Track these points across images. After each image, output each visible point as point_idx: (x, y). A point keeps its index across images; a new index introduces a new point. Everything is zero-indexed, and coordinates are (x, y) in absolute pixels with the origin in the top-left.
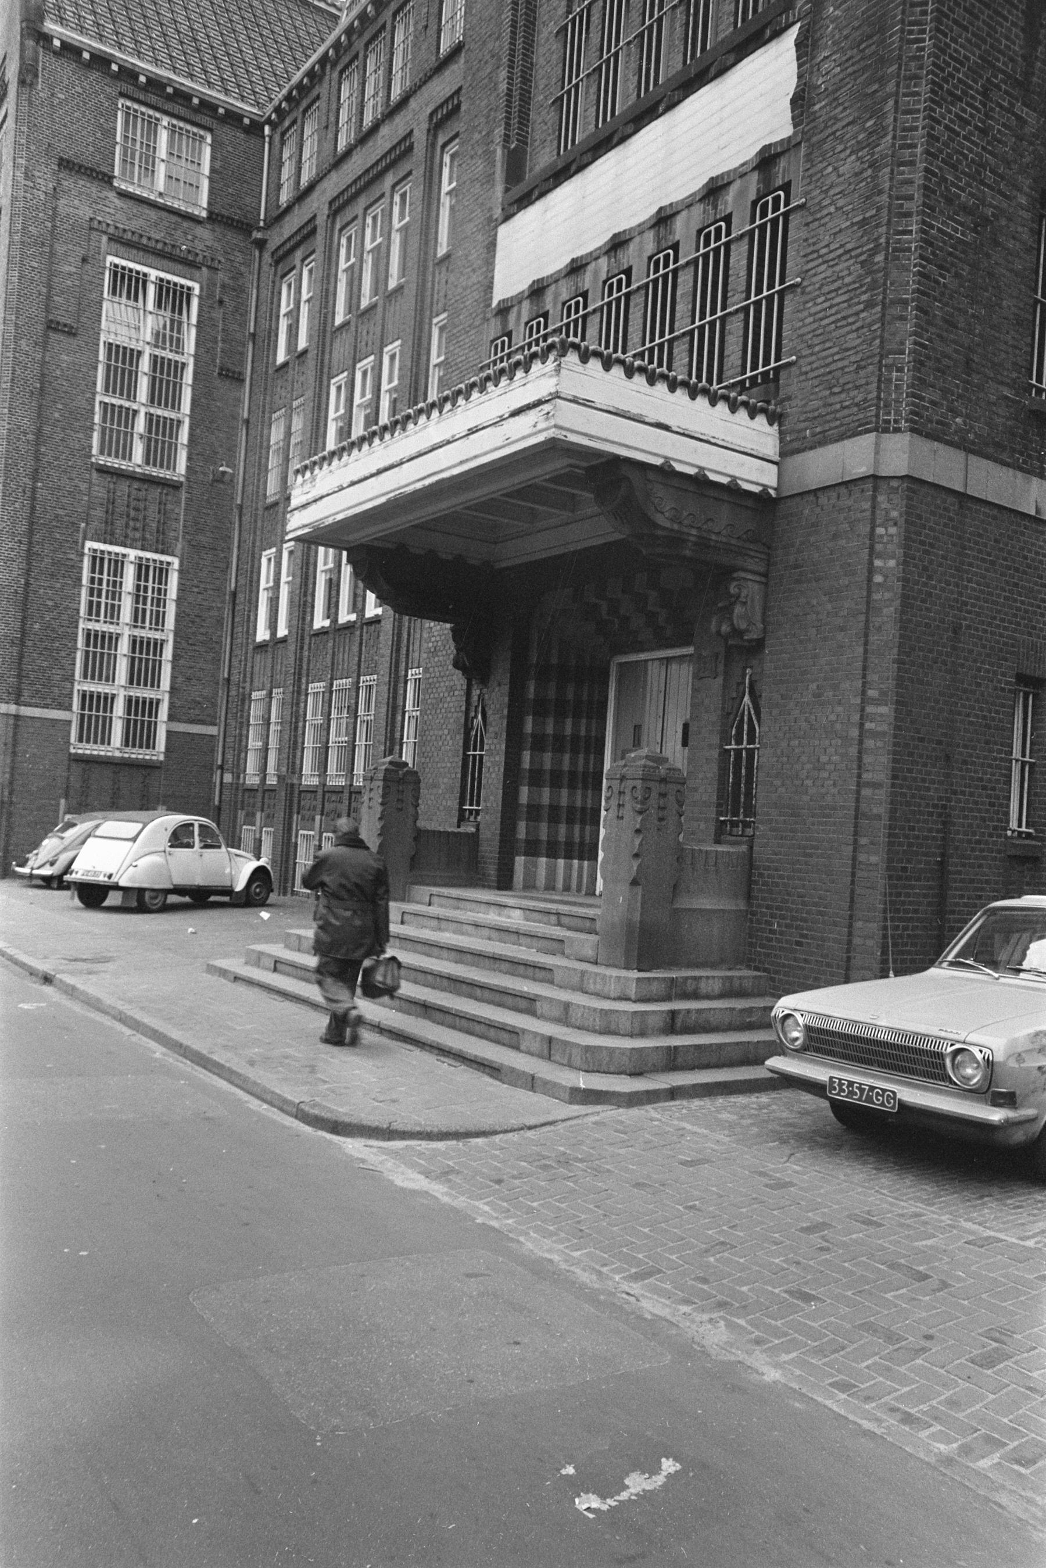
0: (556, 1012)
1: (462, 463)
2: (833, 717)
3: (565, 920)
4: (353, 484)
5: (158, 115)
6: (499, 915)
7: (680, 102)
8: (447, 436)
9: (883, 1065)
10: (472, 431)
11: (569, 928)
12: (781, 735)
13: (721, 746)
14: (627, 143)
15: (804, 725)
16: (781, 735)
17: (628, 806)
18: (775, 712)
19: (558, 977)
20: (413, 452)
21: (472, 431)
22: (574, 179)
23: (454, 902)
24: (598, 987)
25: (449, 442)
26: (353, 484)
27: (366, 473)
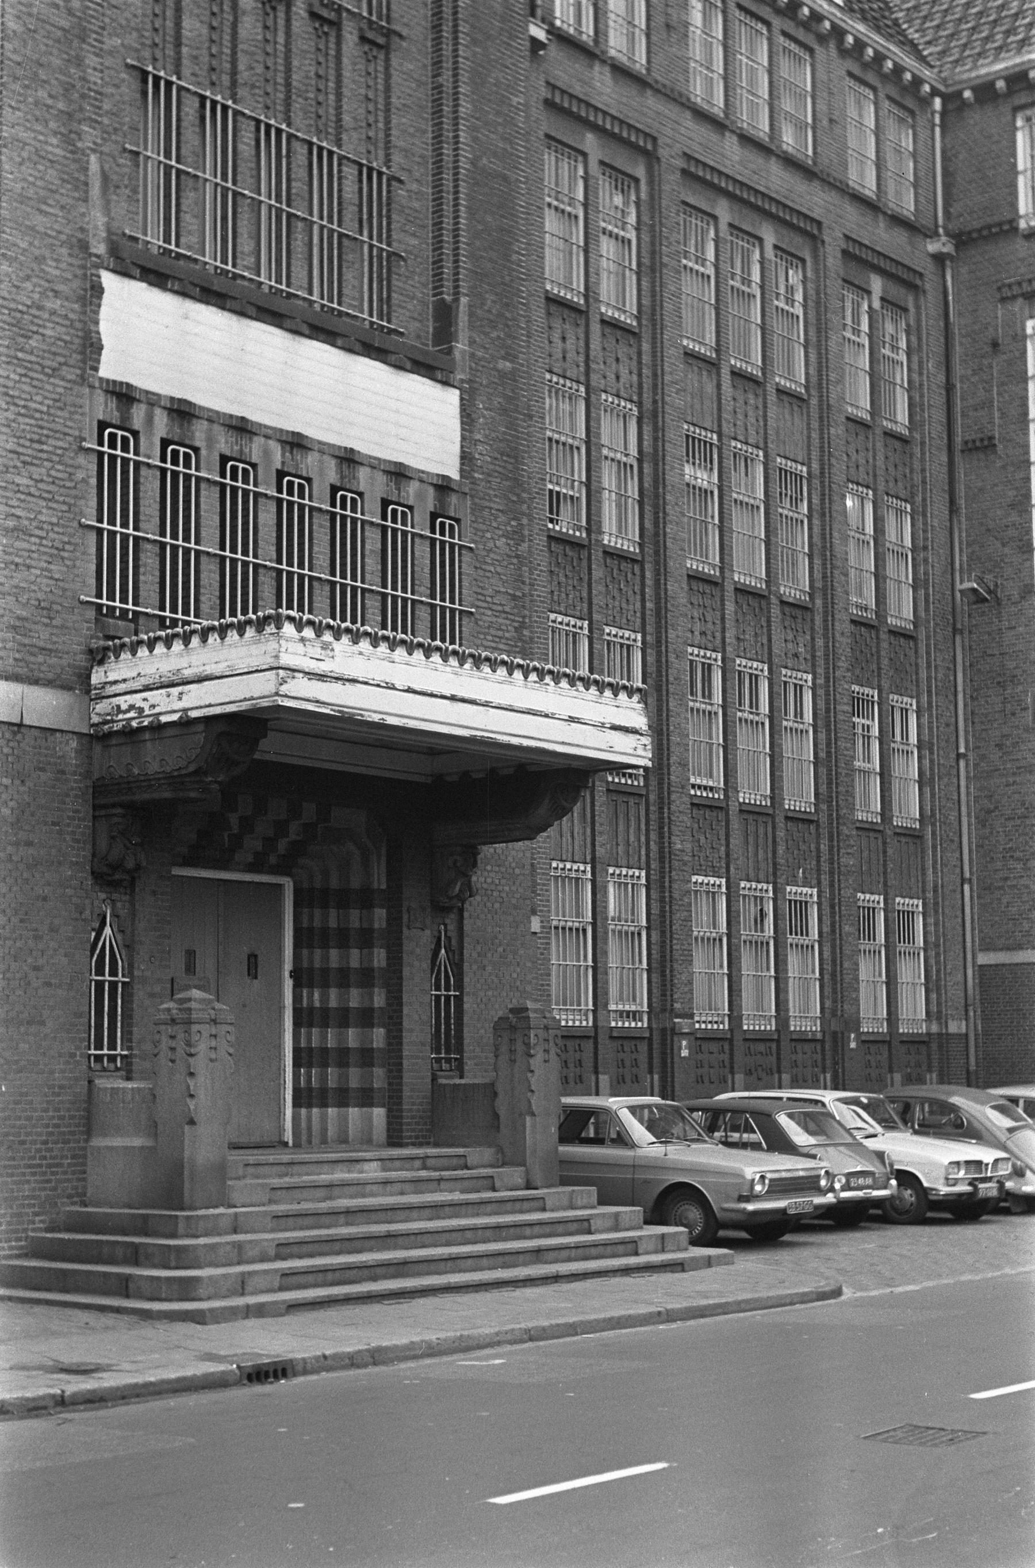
0: (609, 1223)
1: (563, 743)
2: (515, 975)
3: (430, 1162)
4: (410, 690)
5: (958, 595)
6: (349, 1172)
7: (358, 354)
8: (549, 710)
9: (796, 1190)
10: (572, 720)
11: (435, 1169)
12: (479, 986)
13: (462, 993)
14: (298, 338)
15: (496, 980)
16: (479, 986)
17: (553, 1052)
18: (475, 967)
19: (549, 1204)
20: (504, 702)
21: (572, 720)
22: (226, 314)
23: (283, 1168)
24: (585, 1201)
25: (546, 716)
26: (410, 690)
27: (436, 690)
